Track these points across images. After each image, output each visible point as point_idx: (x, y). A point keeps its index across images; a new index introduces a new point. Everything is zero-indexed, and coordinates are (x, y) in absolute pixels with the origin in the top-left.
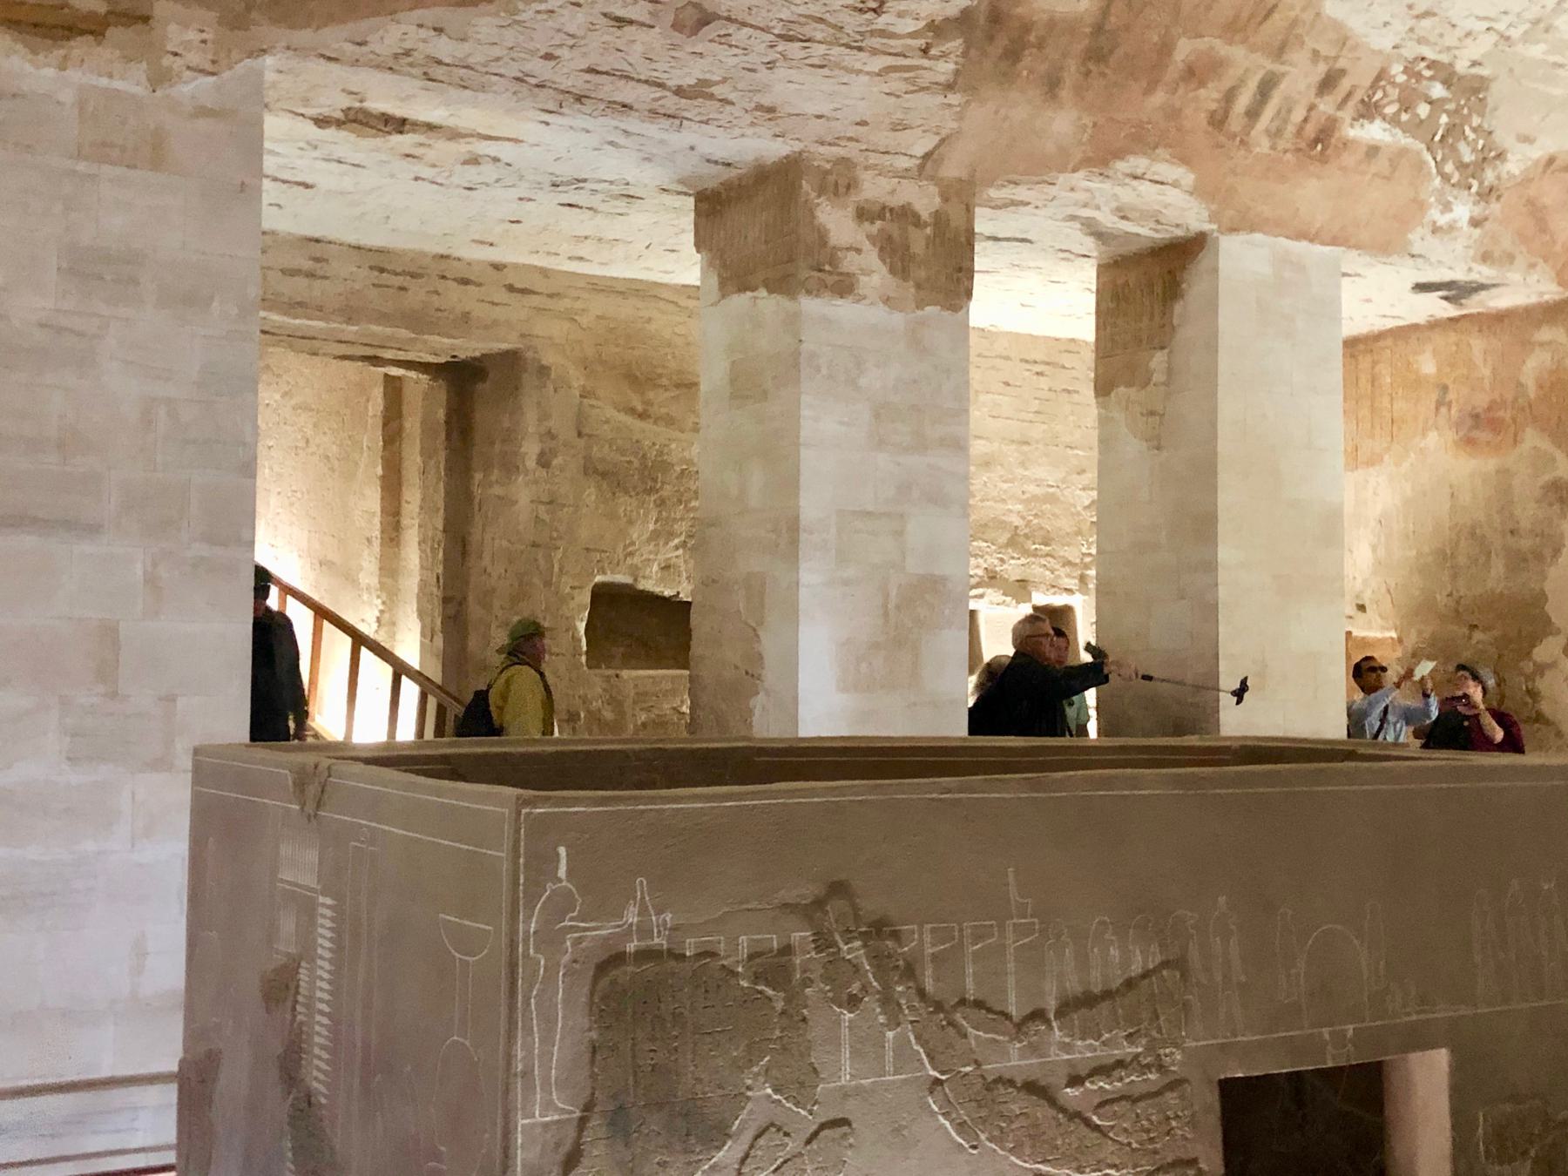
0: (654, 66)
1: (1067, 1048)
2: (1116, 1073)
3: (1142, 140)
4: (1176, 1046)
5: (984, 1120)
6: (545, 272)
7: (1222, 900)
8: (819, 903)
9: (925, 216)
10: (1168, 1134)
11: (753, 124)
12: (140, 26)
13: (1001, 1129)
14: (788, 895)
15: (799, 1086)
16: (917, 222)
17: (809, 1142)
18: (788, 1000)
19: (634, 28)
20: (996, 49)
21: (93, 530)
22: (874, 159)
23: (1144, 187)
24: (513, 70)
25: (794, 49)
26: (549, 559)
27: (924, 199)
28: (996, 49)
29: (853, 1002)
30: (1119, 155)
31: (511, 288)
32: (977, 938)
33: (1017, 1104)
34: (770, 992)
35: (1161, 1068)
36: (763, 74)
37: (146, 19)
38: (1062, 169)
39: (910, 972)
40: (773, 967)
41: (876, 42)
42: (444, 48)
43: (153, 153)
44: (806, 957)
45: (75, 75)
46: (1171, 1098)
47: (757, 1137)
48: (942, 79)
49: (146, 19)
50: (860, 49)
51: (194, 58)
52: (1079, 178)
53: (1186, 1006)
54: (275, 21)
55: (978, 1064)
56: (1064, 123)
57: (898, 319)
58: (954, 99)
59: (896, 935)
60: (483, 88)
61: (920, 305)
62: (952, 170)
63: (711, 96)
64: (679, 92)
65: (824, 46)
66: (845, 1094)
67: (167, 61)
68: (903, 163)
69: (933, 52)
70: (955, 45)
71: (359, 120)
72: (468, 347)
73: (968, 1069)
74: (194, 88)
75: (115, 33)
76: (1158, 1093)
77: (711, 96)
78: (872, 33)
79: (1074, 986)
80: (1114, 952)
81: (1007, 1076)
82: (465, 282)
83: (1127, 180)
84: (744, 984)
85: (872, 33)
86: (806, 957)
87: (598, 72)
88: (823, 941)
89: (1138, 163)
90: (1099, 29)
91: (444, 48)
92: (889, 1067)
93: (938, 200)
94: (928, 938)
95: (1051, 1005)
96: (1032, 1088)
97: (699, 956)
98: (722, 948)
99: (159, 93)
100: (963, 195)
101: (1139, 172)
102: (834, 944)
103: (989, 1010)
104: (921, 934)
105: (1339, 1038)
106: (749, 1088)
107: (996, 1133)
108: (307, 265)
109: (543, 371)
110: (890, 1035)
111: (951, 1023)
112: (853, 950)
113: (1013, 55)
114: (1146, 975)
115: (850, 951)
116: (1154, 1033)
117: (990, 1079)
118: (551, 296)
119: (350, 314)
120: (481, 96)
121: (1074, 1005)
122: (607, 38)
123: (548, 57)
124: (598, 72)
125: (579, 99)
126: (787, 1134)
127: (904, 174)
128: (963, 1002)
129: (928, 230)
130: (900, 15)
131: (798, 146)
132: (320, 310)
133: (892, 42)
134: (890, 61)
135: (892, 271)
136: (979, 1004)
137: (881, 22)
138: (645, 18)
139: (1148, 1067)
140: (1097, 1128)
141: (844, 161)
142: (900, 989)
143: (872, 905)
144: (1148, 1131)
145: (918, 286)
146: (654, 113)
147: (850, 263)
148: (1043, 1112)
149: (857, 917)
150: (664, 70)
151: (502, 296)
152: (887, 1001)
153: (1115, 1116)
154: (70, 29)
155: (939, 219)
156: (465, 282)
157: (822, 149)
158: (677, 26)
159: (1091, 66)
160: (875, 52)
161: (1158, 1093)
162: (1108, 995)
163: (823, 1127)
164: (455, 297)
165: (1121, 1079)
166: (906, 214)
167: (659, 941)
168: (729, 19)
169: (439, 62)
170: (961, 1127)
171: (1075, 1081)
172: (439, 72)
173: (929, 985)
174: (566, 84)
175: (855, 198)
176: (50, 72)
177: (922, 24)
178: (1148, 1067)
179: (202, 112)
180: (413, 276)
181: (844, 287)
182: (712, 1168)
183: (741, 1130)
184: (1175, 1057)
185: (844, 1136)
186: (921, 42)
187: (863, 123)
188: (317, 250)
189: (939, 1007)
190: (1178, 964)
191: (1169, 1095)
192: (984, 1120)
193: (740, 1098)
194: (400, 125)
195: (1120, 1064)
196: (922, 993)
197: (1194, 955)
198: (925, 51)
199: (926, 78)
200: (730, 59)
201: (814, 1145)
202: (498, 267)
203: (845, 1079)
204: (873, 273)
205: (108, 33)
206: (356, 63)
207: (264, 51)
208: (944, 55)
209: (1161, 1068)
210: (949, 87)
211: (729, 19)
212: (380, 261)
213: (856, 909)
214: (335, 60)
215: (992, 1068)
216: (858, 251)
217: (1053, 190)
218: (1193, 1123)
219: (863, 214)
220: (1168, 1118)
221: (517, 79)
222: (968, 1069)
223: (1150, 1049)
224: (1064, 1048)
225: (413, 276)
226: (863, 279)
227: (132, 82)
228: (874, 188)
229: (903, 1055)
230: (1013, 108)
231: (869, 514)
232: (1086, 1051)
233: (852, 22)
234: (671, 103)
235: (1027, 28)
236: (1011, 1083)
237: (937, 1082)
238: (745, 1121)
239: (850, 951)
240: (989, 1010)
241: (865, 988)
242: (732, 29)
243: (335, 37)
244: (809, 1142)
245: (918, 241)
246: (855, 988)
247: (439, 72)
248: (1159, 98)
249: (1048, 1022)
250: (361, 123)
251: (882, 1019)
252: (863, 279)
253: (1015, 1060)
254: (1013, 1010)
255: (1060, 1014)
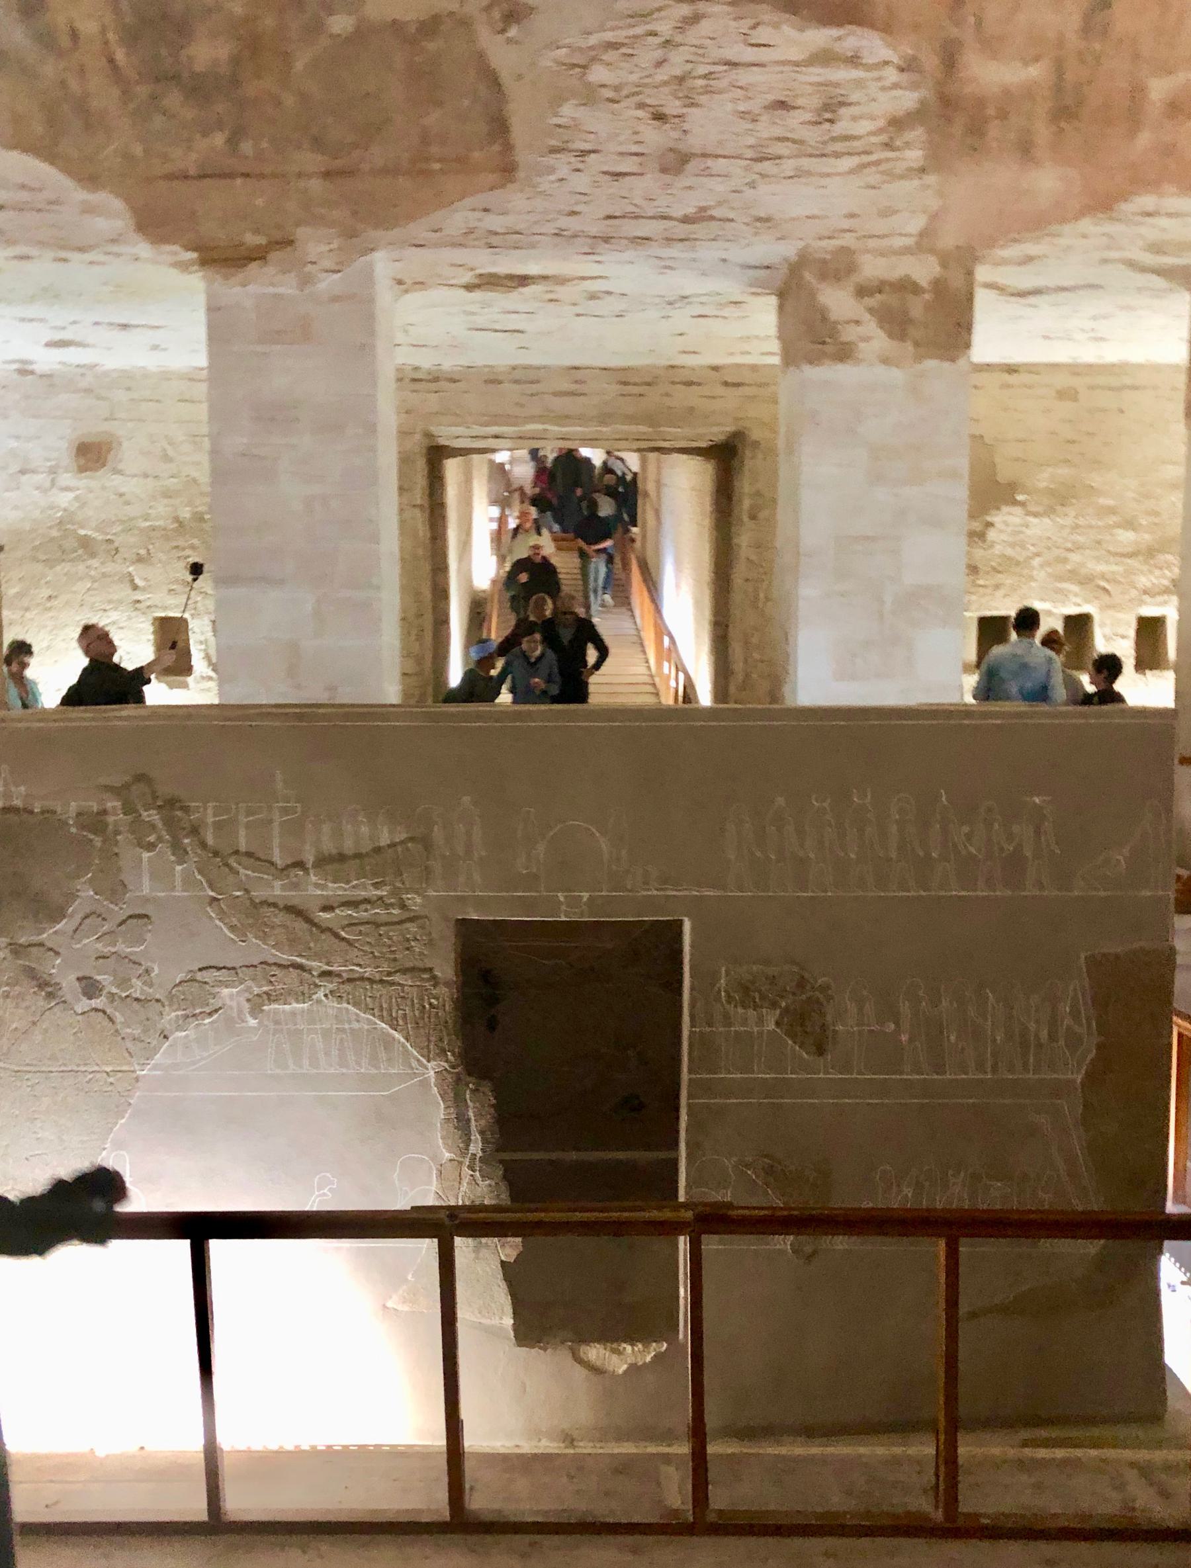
0: (656, 203)
1: (317, 886)
2: (363, 907)
3: (1141, 180)
4: (417, 893)
5: (251, 926)
6: (754, 368)
7: (466, 799)
8: (126, 786)
9: (924, 283)
10: (408, 949)
11: (756, 234)
12: (289, 248)
13: (265, 933)
14: (103, 780)
15: (116, 890)
16: (915, 289)
17: (120, 924)
18: (104, 842)
19: (628, 178)
20: (958, 129)
21: (281, 582)
22: (872, 243)
23: (1163, 222)
24: (550, 228)
25: (766, 166)
26: (756, 590)
27: (923, 270)
28: (958, 129)
29: (151, 847)
30: (1124, 196)
31: (726, 384)
32: (249, 813)
33: (280, 918)
34: (92, 837)
35: (403, 906)
36: (749, 193)
37: (291, 243)
38: (1064, 221)
39: (195, 831)
40: (95, 822)
41: (839, 147)
42: (494, 222)
43: (302, 332)
44: (117, 817)
45: (251, 288)
46: (412, 927)
47: (86, 917)
48: (915, 165)
49: (291, 243)
50: (823, 155)
51: (328, 263)
52: (1086, 225)
53: (428, 870)
54: (376, 226)
55: (247, 891)
56: (1047, 181)
57: (896, 375)
58: (931, 179)
59: (186, 809)
60: (533, 246)
61: (919, 358)
62: (949, 239)
63: (712, 218)
64: (686, 220)
65: (792, 161)
66: (146, 900)
67: (309, 267)
68: (899, 242)
69: (898, 143)
70: (917, 134)
71: (489, 282)
72: (717, 433)
73: (238, 893)
74: (327, 284)
75: (274, 256)
76: (401, 922)
77: (712, 218)
78: (833, 139)
79: (328, 847)
80: (364, 829)
81: (271, 900)
82: (690, 384)
83: (1139, 218)
84: (73, 830)
85: (833, 139)
86: (117, 817)
87: (615, 217)
88: (128, 809)
89: (1147, 201)
90: (1058, 88)
91: (494, 222)
92: (179, 888)
93: (938, 269)
94: (210, 811)
95: (310, 859)
96: (291, 910)
97: (43, 812)
98: (59, 810)
99: (307, 291)
100: (964, 260)
101: (1150, 209)
102: (136, 811)
103: (259, 859)
104: (205, 809)
105: (574, 902)
106: (78, 891)
107: (261, 934)
108: (574, 387)
109: (756, 444)
110: (178, 868)
111: (227, 865)
112: (152, 816)
113: (976, 129)
114: (392, 845)
115: (149, 816)
116: (399, 885)
117: (257, 901)
118: (760, 385)
119: (605, 418)
120: (532, 251)
121: (322, 861)
122: (611, 191)
123: (573, 213)
124: (615, 217)
125: (607, 240)
126: (104, 919)
127: (906, 251)
128: (237, 852)
129: (927, 296)
130: (854, 119)
131: (801, 244)
132: (581, 419)
133: (856, 144)
134: (854, 161)
135: (891, 335)
136: (249, 854)
137: (840, 128)
138: (634, 169)
139: (392, 905)
140: (343, 939)
141: (845, 251)
142: (186, 841)
143: (166, 790)
144: (390, 946)
145: (917, 344)
146: (669, 240)
147: (849, 334)
148: (300, 925)
149: (155, 798)
150: (662, 204)
151: (720, 390)
152: (177, 847)
153: (360, 933)
154: (245, 258)
155: (939, 286)
156: (690, 384)
157: (824, 243)
158: (664, 170)
159: (1063, 124)
160: (837, 155)
161: (401, 922)
162: (358, 856)
163: (130, 917)
164: (683, 397)
165: (366, 910)
166: (907, 286)
167: (18, 803)
168: (704, 155)
169: (496, 234)
170: (232, 928)
171: (327, 908)
172: (494, 240)
173: (210, 840)
174: (594, 230)
175: (856, 278)
176: (238, 289)
177: (881, 123)
178: (392, 905)
179: (335, 299)
180: (649, 384)
181: (844, 353)
182: (55, 932)
183: (72, 916)
184: (415, 901)
185: (145, 925)
186: (883, 138)
187: (852, 216)
188: (579, 375)
189: (216, 854)
190: (426, 843)
191: (408, 925)
192: (251, 926)
193: (72, 896)
194: (524, 280)
195: (367, 901)
196: (203, 845)
197: (438, 834)
198: (888, 146)
199: (900, 167)
200: (719, 187)
201: (123, 927)
202: (716, 368)
203: (146, 890)
204: (873, 339)
205: (269, 257)
206: (437, 245)
207: (372, 250)
208: (908, 145)
209: (403, 906)
210: (923, 170)
211: (704, 155)
212: (624, 377)
213: (153, 792)
214: (421, 246)
215: (258, 894)
216: (857, 322)
217: (1063, 241)
218: (430, 943)
219: (862, 292)
220: (408, 940)
221: (556, 234)
222: (238, 893)
223: (393, 893)
224: (315, 888)
225: (649, 384)
226: (862, 345)
227: (287, 287)
228: (872, 268)
229: (188, 882)
230: (993, 180)
231: (867, 538)
232: (335, 890)
233: (812, 136)
234: (681, 230)
235: (981, 103)
236: (275, 905)
237: (215, 899)
238: (76, 909)
239: (149, 816)
240: (259, 859)
241: (160, 839)
242: (710, 162)
243: (418, 229)
244: (120, 924)
245: (917, 308)
246: (152, 838)
247: (494, 240)
248: (1144, 139)
249: (306, 870)
250: (493, 284)
251: (173, 858)
252: (862, 345)
253: (277, 890)
254: (280, 862)
255: (314, 866)
